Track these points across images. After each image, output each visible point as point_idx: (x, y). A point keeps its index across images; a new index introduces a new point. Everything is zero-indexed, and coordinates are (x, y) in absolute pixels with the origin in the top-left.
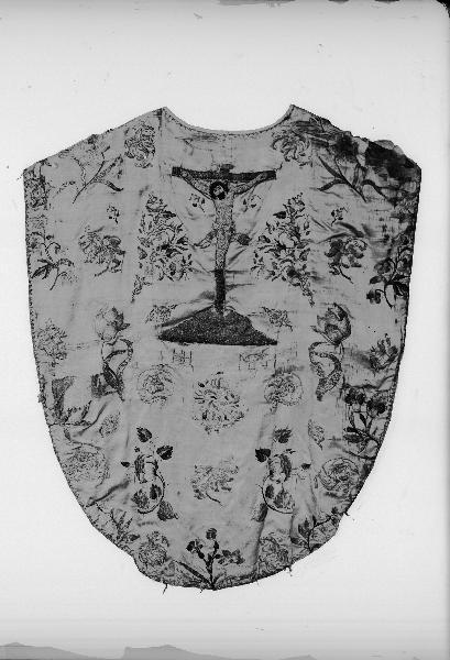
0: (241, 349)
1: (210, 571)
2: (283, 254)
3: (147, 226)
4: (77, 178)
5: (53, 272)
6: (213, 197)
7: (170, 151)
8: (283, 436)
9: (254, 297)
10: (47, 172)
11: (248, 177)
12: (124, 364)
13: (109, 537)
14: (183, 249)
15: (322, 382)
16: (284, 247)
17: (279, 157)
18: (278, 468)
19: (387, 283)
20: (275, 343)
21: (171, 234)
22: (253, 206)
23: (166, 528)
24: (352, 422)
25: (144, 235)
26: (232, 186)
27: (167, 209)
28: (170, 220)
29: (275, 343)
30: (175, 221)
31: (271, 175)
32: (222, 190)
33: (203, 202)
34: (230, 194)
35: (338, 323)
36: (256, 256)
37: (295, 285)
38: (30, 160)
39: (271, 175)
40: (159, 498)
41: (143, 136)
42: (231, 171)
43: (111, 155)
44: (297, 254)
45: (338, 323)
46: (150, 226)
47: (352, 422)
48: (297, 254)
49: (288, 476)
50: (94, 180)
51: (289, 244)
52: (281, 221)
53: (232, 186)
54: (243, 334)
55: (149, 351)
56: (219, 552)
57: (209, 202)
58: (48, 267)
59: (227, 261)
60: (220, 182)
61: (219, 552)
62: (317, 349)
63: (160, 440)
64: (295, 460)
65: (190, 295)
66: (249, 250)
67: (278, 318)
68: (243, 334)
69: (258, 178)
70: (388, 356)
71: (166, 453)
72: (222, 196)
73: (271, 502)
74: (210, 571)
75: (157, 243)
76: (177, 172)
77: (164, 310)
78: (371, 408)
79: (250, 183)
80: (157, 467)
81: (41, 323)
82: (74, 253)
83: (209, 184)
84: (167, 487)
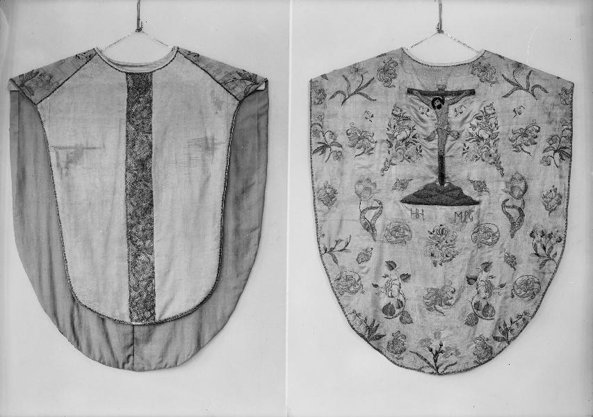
0: (457, 209)
1: (436, 361)
2: (482, 143)
3: (392, 126)
4: (344, 89)
5: (328, 150)
6: (434, 107)
7: (406, 78)
8: (487, 266)
9: (464, 172)
10: (325, 85)
11: (459, 93)
12: (376, 216)
13: (362, 336)
14: (416, 142)
15: (513, 224)
16: (482, 139)
17: (477, 80)
18: (482, 289)
19: (555, 152)
20: (477, 203)
21: (408, 132)
22: (461, 113)
23: (406, 329)
24: (536, 250)
25: (390, 132)
26: (447, 99)
27: (405, 115)
28: (407, 123)
29: (477, 203)
30: (412, 124)
31: (472, 92)
32: (439, 103)
33: (428, 110)
34: (446, 104)
35: (519, 188)
36: (465, 145)
37: (491, 164)
38: (316, 74)
39: (472, 92)
40: (402, 309)
41: (388, 66)
42: (446, 90)
43: (367, 78)
44: (491, 142)
45: (519, 188)
46: (395, 127)
47: (536, 250)
48: (491, 142)
49: (490, 295)
50: (355, 93)
51: (486, 136)
52: (479, 121)
53: (447, 99)
54: (455, 197)
55: (394, 210)
56: (443, 348)
57: (432, 112)
58: (324, 147)
59: (446, 150)
60: (438, 99)
61: (443, 348)
62: (507, 204)
63: (403, 270)
64: (496, 283)
65: (421, 173)
66: (459, 144)
67: (481, 186)
68: (455, 197)
69: (464, 94)
70: (557, 201)
71: (406, 277)
72: (439, 107)
73: (480, 313)
74: (436, 361)
75: (400, 137)
76: (410, 91)
77: (403, 185)
78: (549, 247)
79: (461, 96)
80: (400, 287)
81: (320, 184)
82: (342, 139)
83: (432, 99)
84: (407, 301)
